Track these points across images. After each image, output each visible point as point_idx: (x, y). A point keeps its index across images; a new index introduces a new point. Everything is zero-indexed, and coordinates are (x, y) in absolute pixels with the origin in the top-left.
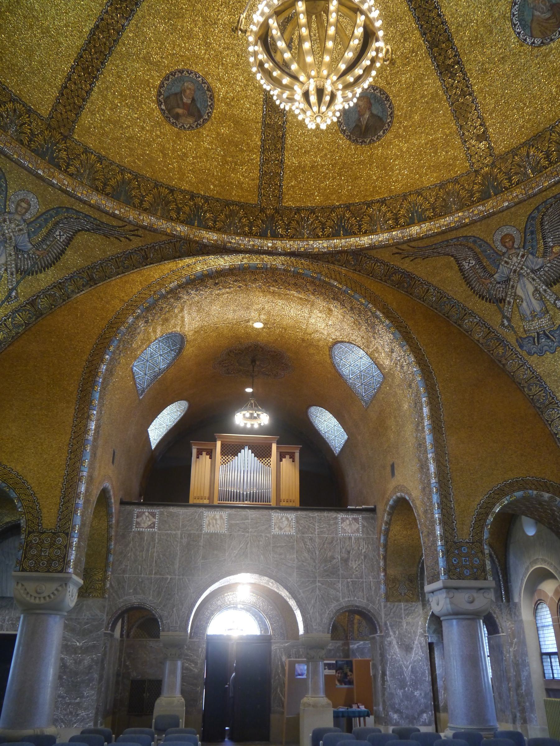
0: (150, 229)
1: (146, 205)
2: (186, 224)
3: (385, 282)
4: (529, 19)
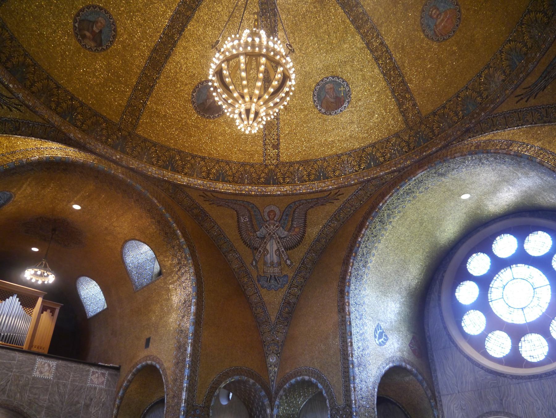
0: (33, 110)
1: (34, 89)
2: (61, 116)
3: (188, 211)
4: (323, 97)
